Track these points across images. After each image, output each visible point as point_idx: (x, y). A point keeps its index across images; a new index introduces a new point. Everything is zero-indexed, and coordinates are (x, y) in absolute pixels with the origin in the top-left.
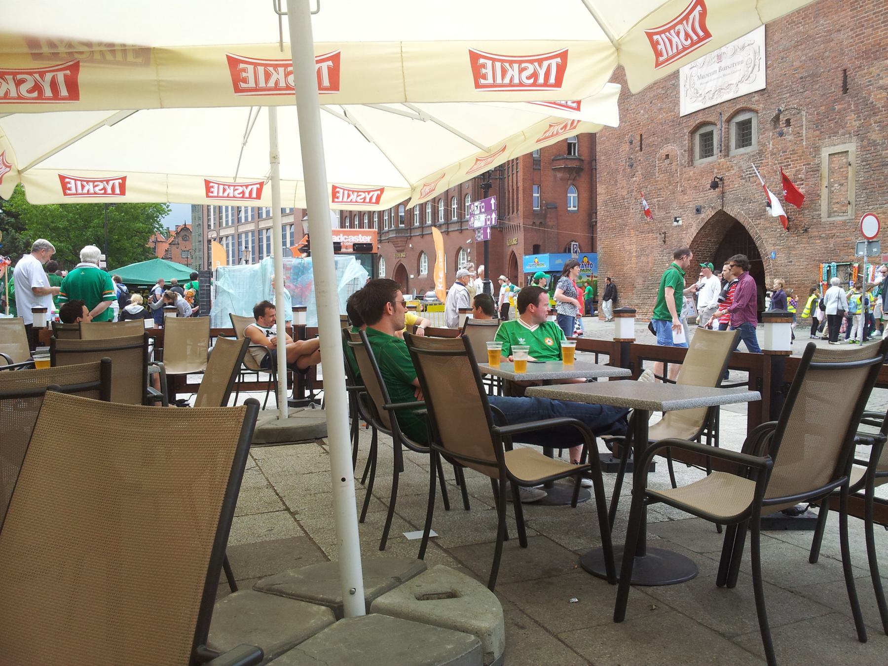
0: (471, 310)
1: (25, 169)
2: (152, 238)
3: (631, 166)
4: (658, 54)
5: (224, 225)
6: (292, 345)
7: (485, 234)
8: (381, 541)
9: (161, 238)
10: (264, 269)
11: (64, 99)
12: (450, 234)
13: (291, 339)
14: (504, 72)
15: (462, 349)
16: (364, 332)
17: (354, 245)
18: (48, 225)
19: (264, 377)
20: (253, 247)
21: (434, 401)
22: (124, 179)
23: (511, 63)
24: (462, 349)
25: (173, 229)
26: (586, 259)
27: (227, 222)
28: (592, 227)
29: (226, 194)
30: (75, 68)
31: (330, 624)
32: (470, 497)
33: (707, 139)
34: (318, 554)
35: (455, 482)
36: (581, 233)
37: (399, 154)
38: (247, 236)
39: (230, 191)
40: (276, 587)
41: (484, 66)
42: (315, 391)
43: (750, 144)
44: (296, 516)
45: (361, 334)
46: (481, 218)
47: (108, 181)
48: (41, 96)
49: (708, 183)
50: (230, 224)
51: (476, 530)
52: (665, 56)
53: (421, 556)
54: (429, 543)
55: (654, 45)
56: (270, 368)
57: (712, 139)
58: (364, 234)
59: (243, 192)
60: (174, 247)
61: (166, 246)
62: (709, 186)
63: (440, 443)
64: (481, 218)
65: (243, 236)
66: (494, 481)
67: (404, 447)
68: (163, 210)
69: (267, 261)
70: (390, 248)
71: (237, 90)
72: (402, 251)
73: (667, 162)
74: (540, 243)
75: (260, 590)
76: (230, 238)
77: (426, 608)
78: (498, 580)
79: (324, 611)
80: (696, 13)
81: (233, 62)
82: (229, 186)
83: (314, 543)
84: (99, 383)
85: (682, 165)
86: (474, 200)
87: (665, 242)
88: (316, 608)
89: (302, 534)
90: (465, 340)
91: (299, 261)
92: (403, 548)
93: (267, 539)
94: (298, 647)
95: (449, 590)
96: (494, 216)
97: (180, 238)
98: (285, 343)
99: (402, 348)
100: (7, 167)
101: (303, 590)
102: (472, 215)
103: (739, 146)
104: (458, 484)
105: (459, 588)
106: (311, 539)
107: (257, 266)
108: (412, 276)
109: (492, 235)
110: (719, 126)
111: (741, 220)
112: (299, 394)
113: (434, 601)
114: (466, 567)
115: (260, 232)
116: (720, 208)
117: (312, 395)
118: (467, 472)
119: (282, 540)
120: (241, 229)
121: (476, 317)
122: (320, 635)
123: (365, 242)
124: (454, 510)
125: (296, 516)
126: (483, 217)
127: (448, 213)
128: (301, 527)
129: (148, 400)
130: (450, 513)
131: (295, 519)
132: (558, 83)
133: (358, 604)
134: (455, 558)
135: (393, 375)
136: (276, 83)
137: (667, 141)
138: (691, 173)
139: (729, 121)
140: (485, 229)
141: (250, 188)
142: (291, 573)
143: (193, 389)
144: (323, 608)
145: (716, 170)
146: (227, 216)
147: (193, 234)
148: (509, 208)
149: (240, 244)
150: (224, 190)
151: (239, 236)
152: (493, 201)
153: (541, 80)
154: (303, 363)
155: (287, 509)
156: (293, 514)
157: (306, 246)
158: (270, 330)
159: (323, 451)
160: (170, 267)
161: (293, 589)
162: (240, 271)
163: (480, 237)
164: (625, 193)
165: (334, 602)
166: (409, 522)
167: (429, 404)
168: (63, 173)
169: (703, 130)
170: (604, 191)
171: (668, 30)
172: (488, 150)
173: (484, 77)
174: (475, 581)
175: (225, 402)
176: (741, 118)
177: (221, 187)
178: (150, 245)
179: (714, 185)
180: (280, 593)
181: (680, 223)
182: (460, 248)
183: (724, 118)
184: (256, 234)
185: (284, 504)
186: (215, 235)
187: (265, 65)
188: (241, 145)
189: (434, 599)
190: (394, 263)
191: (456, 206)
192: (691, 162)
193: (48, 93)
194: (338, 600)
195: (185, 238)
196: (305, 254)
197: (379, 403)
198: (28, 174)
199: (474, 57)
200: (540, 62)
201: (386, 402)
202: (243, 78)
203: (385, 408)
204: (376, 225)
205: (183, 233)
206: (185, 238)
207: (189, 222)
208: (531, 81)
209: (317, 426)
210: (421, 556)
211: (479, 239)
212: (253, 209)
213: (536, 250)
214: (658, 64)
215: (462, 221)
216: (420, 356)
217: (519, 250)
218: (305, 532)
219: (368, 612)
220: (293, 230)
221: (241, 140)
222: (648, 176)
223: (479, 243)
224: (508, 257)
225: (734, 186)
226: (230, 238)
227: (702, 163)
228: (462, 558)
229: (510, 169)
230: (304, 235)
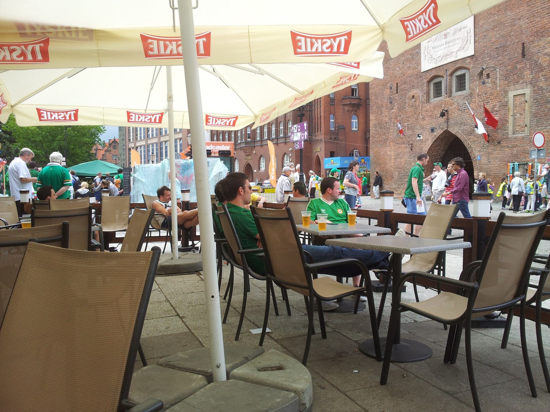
1: (16, 105)
2: (94, 147)
3: (391, 103)
4: (408, 33)
6: (181, 213)
7: (301, 145)
8: (236, 335)
9: (100, 147)
10: (163, 166)
11: (40, 61)
13: (180, 210)
14: (312, 45)
15: (286, 216)
16: (226, 206)
17: (220, 151)
18: (30, 139)
19: (164, 233)
21: (269, 248)
22: (77, 111)
23: (316, 39)
24: (286, 216)
25: (107, 141)
26: (363, 160)
27: (141, 137)
28: (367, 140)
30: (46, 42)
31: (204, 386)
32: (291, 308)
33: (438, 86)
34: (197, 342)
35: (282, 298)
36: (360, 144)
37: (247, 95)
38: (153, 146)
39: (142, 118)
40: (171, 363)
41: (300, 41)
42: (195, 242)
43: (465, 89)
44: (183, 319)
45: (223, 207)
46: (298, 135)
47: (67, 112)
48: (25, 60)
49: (438, 113)
50: (142, 138)
51: (295, 328)
52: (412, 35)
53: (261, 344)
54: (266, 336)
55: (405, 28)
56: (167, 228)
57: (441, 86)
58: (225, 145)
59: (151, 119)
60: (108, 153)
61: (103, 152)
62: (439, 115)
63: (273, 274)
64: (298, 135)
65: (151, 146)
66: (306, 298)
67: (250, 277)
68: (101, 130)
69: (165, 161)
70: (242, 154)
71: (147, 55)
72: (249, 155)
73: (413, 100)
74: (334, 150)
75: (161, 365)
76: (143, 147)
77: (264, 376)
79: (201, 378)
80: (431, 8)
81: (144, 38)
82: (142, 115)
83: (195, 336)
84: (61, 237)
85: (422, 102)
86: (293, 124)
87: (412, 149)
88: (195, 376)
89: (187, 330)
90: (288, 210)
91: (185, 161)
93: (166, 334)
94: (185, 400)
95: (278, 365)
96: (306, 133)
97: (112, 148)
98: (176, 212)
99: (249, 215)
100: (4, 103)
101: (188, 365)
102: (293, 133)
103: (457, 90)
104: (284, 299)
105: (284, 363)
106: (192, 333)
107: (159, 165)
108: (255, 171)
109: (304, 145)
110: (445, 78)
111: (459, 136)
112: (185, 244)
113: (269, 372)
115: (161, 143)
116: (446, 129)
117: (193, 245)
118: (290, 292)
119: (175, 334)
120: (149, 142)
121: (295, 196)
122: (198, 393)
123: (226, 150)
124: (281, 315)
125: (183, 319)
126: (299, 134)
127: (277, 132)
128: (187, 326)
129: (92, 248)
130: (279, 317)
131: (183, 321)
132: (346, 51)
133: (222, 374)
134: (282, 345)
135: (244, 232)
136: (171, 51)
137: (413, 87)
138: (428, 107)
139: (451, 75)
140: (300, 142)
141: (155, 116)
142: (180, 355)
143: (120, 240)
144: (200, 376)
145: (443, 105)
146: (141, 134)
148: (315, 128)
149: (148, 151)
151: (148, 146)
152: (305, 124)
153: (335, 50)
154: (188, 225)
155: (178, 315)
156: (181, 318)
157: (189, 152)
158: (167, 204)
159: (200, 279)
160: (105, 165)
161: (182, 364)
162: (149, 167)
163: (298, 147)
164: (387, 119)
165: (207, 373)
166: (254, 323)
167: (266, 250)
168: (39, 107)
169: (436, 81)
170: (374, 118)
171: (414, 18)
172: (302, 93)
173: (300, 48)
175: (139, 249)
176: (459, 73)
177: (137, 116)
178: (93, 151)
179: (442, 115)
180: (174, 367)
181: (421, 138)
182: (285, 154)
183: (449, 73)
184: (159, 145)
185: (176, 311)
186: (133, 145)
187: (164, 40)
188: (149, 90)
190: (244, 162)
191: (282, 128)
192: (428, 100)
194: (209, 371)
195: (115, 147)
196: (189, 157)
197: (235, 250)
198: (17, 108)
199: (294, 35)
200: (335, 38)
201: (239, 249)
202: (150, 48)
203: (238, 253)
204: (233, 139)
205: (113, 144)
206: (115, 147)
207: (117, 137)
208: (329, 50)
209: (196, 264)
210: (261, 344)
211: (297, 148)
213: (332, 155)
214: (407, 40)
215: (286, 137)
216: (260, 219)
217: (321, 155)
218: (189, 329)
220: (181, 142)
221: (150, 87)
222: (401, 109)
223: (296, 150)
224: (315, 159)
225: (455, 115)
226: (143, 147)
227: (435, 101)
228: (286, 345)
229: (316, 105)
230: (188, 145)
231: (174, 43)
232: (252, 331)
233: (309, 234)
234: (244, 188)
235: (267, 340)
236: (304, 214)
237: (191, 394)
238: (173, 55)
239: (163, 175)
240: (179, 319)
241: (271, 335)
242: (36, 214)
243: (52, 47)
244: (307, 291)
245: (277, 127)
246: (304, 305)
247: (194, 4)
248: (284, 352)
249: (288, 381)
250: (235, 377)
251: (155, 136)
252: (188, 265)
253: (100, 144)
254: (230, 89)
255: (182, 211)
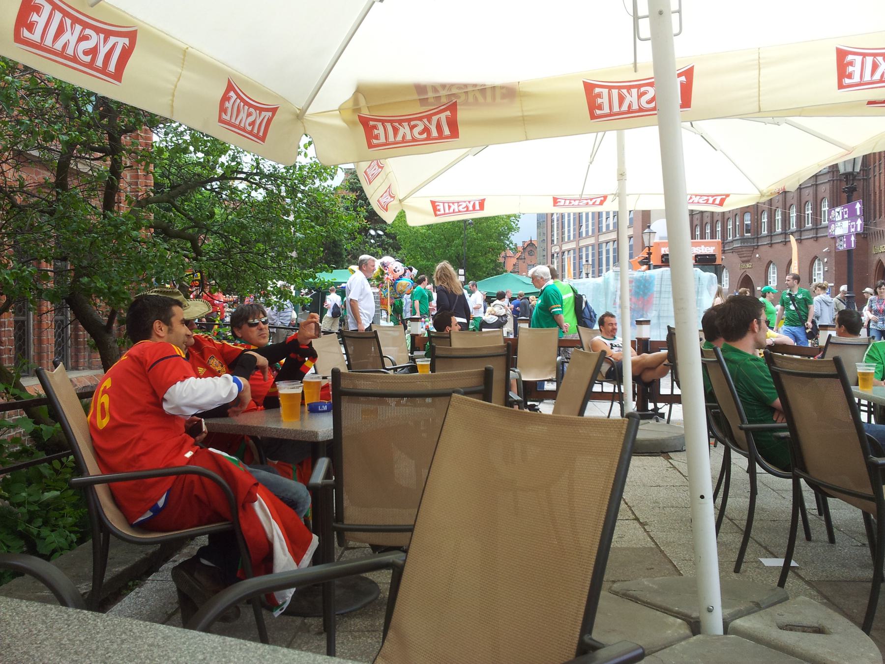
0: (834, 326)
1: (405, 198)
2: (503, 254)
5: (566, 240)
6: (637, 358)
7: (849, 242)
8: (737, 563)
9: (510, 253)
10: (606, 283)
11: (447, 137)
12: (804, 242)
13: (635, 353)
15: (833, 370)
16: (719, 349)
18: (418, 245)
19: (609, 388)
20: (593, 260)
21: (798, 425)
22: (483, 200)
24: (833, 370)
25: (520, 245)
27: (569, 237)
29: (399, 138)
30: (453, 107)
31: (686, 638)
32: (835, 530)
34: (669, 566)
35: (816, 512)
37: (745, 163)
38: (587, 250)
40: (631, 593)
42: (659, 405)
44: (646, 527)
45: (715, 350)
46: (843, 225)
48: (429, 138)
50: (572, 238)
51: (843, 566)
53: (782, 583)
54: (790, 573)
56: (615, 380)
58: (707, 244)
60: (521, 262)
61: (514, 261)
63: (804, 469)
64: (843, 225)
65: (584, 249)
66: (866, 515)
67: (759, 469)
68: (513, 228)
69: (609, 275)
70: (735, 259)
72: (748, 261)
75: (616, 593)
77: (790, 638)
78: (875, 624)
79: (680, 624)
81: (589, 87)
83: (665, 556)
84: (482, 387)
86: (833, 205)
88: (671, 619)
89: (652, 545)
90: (837, 361)
91: (641, 274)
92: (760, 574)
93: (619, 546)
94: (656, 654)
95: (816, 625)
96: (859, 222)
98: (629, 357)
99: (760, 367)
100: (392, 197)
101: (658, 600)
102: (832, 221)
104: (820, 514)
105: (827, 624)
106: (661, 551)
107: (599, 280)
108: (759, 288)
109: (857, 243)
112: (642, 406)
113: (799, 633)
114: (834, 604)
115: (600, 245)
117: (656, 409)
118: (835, 504)
119: (633, 549)
120: (583, 243)
121: (839, 334)
122: (677, 647)
123: (708, 253)
124: (816, 541)
125: (646, 527)
126: (846, 224)
127: (800, 219)
128: (652, 538)
129: (509, 402)
130: (812, 544)
131: (645, 530)
133: (715, 622)
134: (819, 592)
135: (750, 395)
140: (848, 237)
142: (646, 582)
143: (552, 395)
144: (679, 621)
146: (569, 231)
147: (538, 249)
148: (875, 211)
149: (581, 258)
150: (396, 131)
151: (580, 250)
152: (858, 206)
154: (648, 376)
155: (637, 519)
156: (643, 524)
157: (646, 258)
158: (614, 342)
159: (669, 465)
160: (518, 280)
161: (649, 597)
162: (584, 284)
163: (842, 246)
165: (690, 617)
166: (765, 548)
167: (792, 426)
168: (433, 199)
173: (850, 76)
174: (846, 620)
175: (581, 412)
178: (501, 260)
180: (636, 600)
182: (815, 258)
184: (596, 247)
185: (633, 513)
186: (558, 250)
187: (619, 88)
189: (799, 631)
190: (739, 274)
191: (810, 212)
193: (435, 134)
194: (694, 615)
195: (531, 253)
196: (645, 267)
197: (735, 424)
198: (406, 202)
199: (841, 54)
201: (742, 422)
202: (600, 105)
203: (741, 428)
204: (719, 234)
205: (529, 249)
206: (531, 253)
207: (534, 238)
209: (663, 440)
210: (782, 583)
211: (841, 248)
212: (574, 214)
215: (817, 227)
216: (782, 375)
218: (656, 544)
219: (726, 631)
220: (632, 243)
221: (589, 159)
223: (839, 254)
224: (874, 268)
228: (830, 592)
229: (877, 169)
230: (644, 247)
231: (634, 91)
232: (763, 560)
233: (869, 403)
234: (759, 323)
235: (791, 580)
236: (862, 368)
237: (666, 647)
238: (632, 112)
239: (606, 295)
240: (638, 525)
241: (799, 571)
242: (438, 353)
243: (462, 115)
244: (873, 505)
245: (786, 208)
246: (862, 528)
247: (676, 29)
248: (825, 604)
249: (837, 656)
250: (737, 632)
251: (590, 233)
252: (649, 440)
253: (511, 249)
254: (719, 152)
255: (638, 354)
